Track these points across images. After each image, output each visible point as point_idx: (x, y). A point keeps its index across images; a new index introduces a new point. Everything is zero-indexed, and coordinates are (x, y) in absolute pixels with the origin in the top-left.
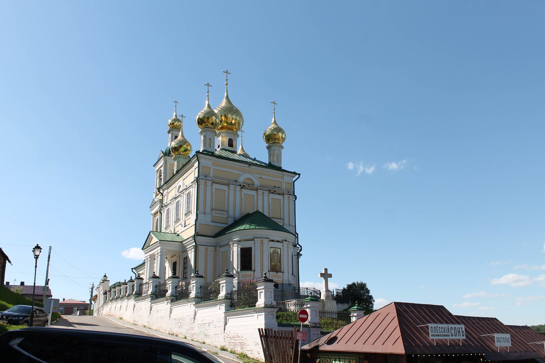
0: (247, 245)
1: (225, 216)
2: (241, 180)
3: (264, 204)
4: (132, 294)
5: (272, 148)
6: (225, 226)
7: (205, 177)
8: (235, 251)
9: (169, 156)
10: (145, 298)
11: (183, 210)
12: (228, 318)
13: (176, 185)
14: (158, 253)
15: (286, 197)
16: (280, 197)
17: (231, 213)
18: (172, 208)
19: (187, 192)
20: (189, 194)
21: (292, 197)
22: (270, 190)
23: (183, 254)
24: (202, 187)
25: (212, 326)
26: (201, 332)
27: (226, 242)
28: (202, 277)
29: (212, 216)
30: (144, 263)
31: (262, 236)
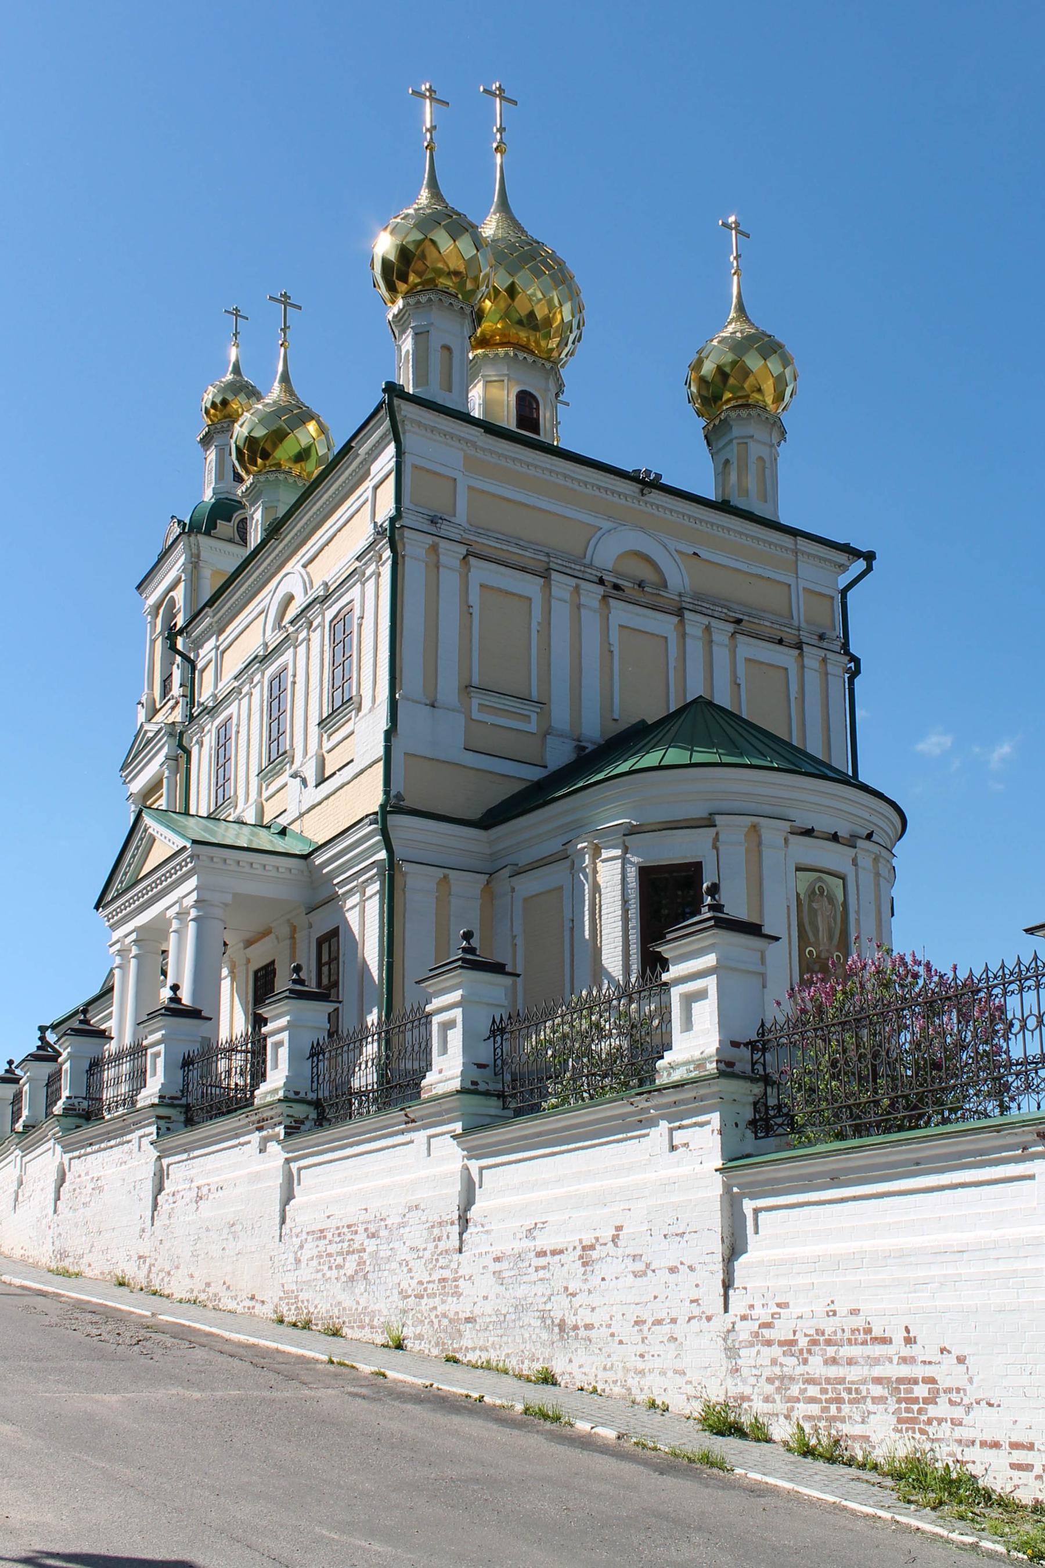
0: (676, 849)
1: (533, 727)
2: (608, 553)
3: (720, 670)
4: (48, 1114)
5: (737, 431)
6: (535, 774)
7: (433, 521)
8: (610, 883)
9: (208, 533)
10: (121, 1131)
11: (308, 703)
12: (748, 1206)
13: (269, 598)
14: (181, 915)
15: (812, 657)
16: (786, 657)
17: (560, 716)
18: (248, 716)
19: (330, 614)
20: (342, 621)
21: (838, 664)
22: (738, 621)
23: (315, 916)
24: (414, 572)
25: (612, 1266)
26: (520, 1307)
27: (553, 846)
28: (498, 968)
29: (470, 719)
30: (107, 991)
31: (752, 807)
